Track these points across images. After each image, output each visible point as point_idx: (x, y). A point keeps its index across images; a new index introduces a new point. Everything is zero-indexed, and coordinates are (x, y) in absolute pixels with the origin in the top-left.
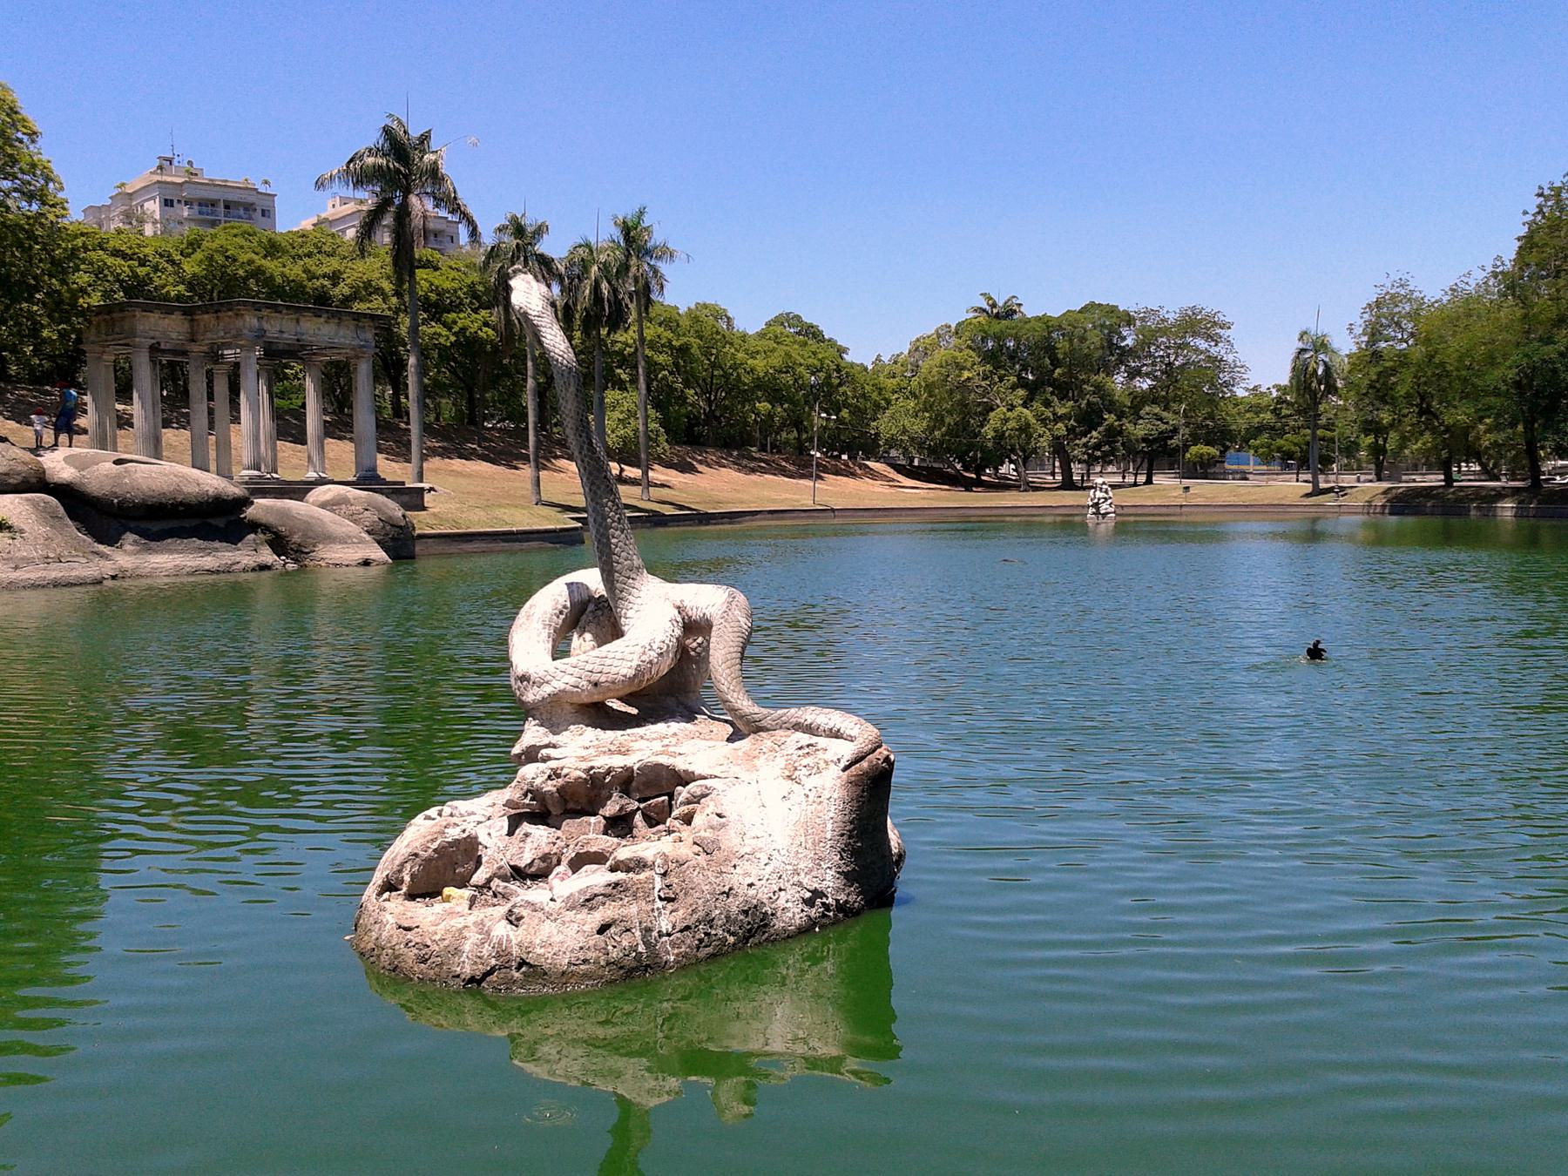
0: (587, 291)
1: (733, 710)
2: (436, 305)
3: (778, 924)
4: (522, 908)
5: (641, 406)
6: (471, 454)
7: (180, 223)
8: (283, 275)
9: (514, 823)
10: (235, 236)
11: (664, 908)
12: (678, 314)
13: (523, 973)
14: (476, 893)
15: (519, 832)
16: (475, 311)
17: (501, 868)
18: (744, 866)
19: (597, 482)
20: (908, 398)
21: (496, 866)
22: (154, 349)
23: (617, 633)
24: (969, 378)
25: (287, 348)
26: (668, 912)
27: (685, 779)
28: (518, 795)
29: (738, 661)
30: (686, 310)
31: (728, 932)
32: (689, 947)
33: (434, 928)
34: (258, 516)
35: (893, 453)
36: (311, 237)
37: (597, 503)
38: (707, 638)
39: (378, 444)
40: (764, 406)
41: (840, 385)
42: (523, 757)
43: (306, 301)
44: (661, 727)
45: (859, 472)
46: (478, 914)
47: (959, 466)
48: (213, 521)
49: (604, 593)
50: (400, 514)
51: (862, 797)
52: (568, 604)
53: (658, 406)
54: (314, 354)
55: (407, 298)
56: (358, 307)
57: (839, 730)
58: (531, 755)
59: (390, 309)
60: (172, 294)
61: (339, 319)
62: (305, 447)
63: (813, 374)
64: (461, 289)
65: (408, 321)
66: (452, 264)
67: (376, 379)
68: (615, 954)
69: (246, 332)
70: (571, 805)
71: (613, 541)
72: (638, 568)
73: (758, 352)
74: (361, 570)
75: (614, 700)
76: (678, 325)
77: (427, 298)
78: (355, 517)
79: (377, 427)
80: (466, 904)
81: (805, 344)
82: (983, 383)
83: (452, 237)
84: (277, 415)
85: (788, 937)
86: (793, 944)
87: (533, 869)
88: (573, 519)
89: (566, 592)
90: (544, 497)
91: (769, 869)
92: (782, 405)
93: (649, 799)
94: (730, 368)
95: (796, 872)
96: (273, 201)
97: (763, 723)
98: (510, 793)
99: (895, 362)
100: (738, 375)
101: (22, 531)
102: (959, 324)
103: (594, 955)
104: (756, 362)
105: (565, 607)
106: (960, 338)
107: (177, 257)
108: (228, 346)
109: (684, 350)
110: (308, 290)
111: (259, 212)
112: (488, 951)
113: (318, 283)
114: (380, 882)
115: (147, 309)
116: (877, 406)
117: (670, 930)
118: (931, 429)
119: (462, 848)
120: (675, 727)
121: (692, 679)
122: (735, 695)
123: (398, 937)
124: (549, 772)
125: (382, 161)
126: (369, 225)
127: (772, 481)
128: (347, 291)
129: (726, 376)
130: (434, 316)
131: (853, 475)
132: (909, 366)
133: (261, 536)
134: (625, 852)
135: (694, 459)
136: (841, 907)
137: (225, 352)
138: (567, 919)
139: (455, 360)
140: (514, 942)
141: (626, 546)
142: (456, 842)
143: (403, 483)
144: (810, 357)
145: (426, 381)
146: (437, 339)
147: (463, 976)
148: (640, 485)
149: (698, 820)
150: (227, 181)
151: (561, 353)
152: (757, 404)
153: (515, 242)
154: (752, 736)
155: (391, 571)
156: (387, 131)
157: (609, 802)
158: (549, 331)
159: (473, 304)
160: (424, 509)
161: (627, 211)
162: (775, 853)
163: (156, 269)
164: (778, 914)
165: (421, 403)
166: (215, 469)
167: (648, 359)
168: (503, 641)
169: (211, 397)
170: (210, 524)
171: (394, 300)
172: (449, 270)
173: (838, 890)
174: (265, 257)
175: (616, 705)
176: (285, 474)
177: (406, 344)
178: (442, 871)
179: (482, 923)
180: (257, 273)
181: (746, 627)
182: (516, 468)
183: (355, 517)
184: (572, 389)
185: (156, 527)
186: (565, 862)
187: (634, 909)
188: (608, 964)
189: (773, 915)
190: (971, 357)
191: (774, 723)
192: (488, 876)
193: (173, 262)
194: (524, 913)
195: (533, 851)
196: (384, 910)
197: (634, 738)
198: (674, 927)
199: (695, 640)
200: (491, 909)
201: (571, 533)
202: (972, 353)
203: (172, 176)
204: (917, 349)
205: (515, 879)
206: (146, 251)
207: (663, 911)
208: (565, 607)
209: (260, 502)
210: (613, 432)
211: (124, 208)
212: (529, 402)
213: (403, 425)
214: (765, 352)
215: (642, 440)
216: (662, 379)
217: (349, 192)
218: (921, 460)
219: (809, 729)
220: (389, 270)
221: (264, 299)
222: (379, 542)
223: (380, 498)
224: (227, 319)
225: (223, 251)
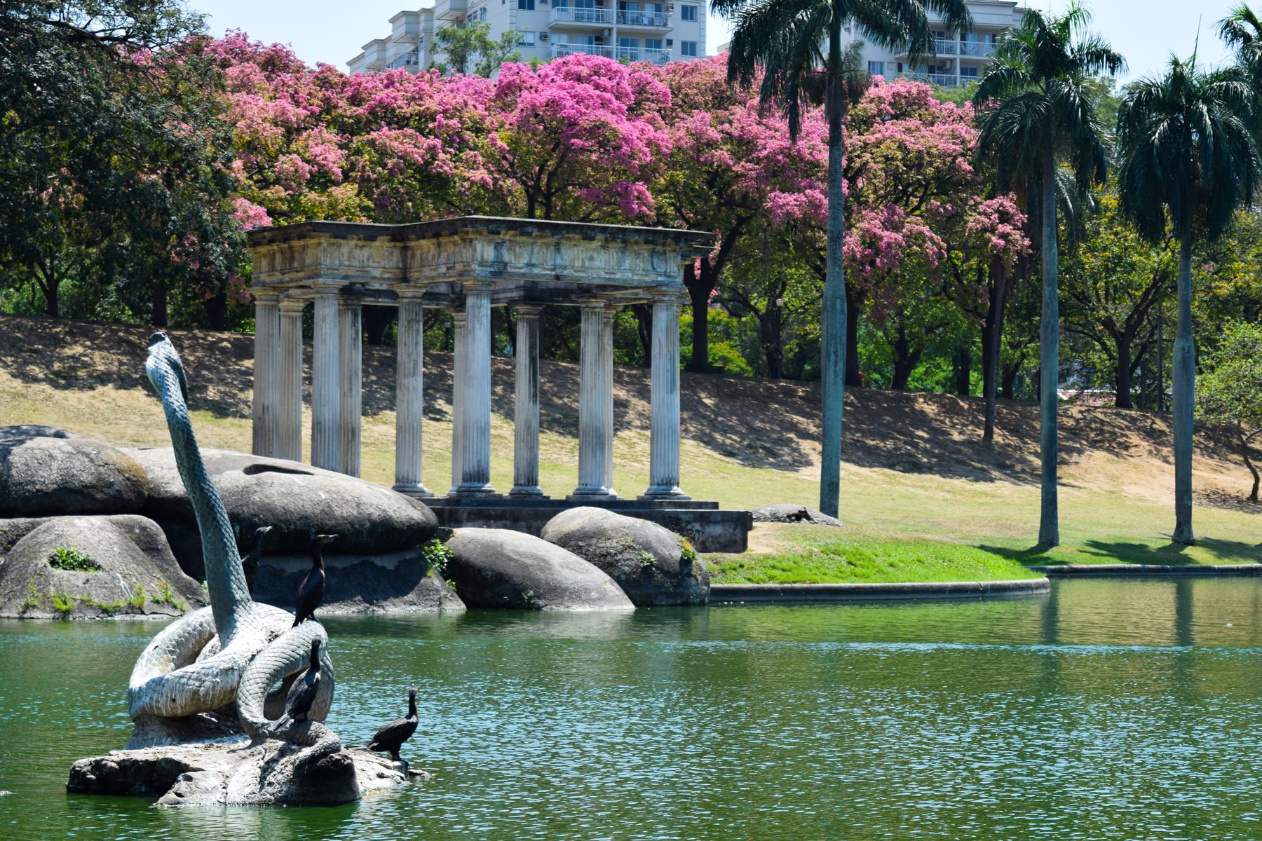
61: (624, 241)
69: (474, 266)
143: (715, 505)
170: (373, 565)
224: (450, 248)
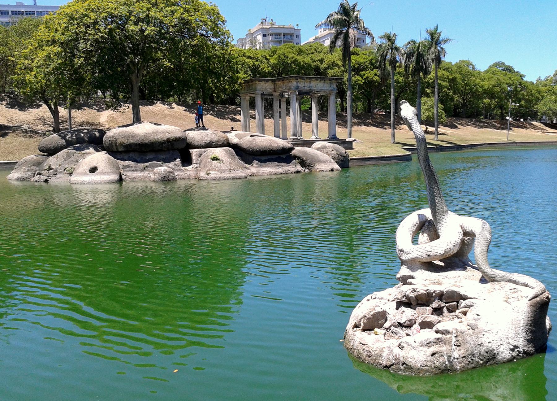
2: (357, 69)
3: (500, 358)
5: (436, 104)
7: (269, 43)
8: (304, 61)
10: (288, 48)
11: (456, 349)
12: (452, 65)
13: (404, 367)
16: (372, 70)
17: (394, 323)
18: (487, 335)
20: (552, 95)
21: (392, 322)
22: (262, 95)
26: (457, 350)
27: (465, 298)
29: (486, 253)
30: (455, 63)
31: (480, 359)
40: (487, 101)
41: (521, 90)
45: (528, 126)
48: (282, 156)
49: (432, 218)
50: (344, 152)
52: (418, 223)
53: (442, 102)
55: (347, 67)
60: (267, 71)
62: (311, 124)
63: (509, 87)
65: (347, 75)
68: (437, 364)
69: (292, 87)
70: (420, 302)
71: (436, 201)
73: (485, 79)
74: (331, 173)
76: (452, 70)
77: (354, 66)
81: (506, 74)
84: (302, 112)
87: (406, 324)
93: (449, 303)
97: (496, 279)
99: (547, 80)
101: (223, 161)
104: (484, 83)
105: (417, 223)
107: (268, 57)
109: (454, 80)
110: (312, 66)
111: (295, 36)
113: (315, 64)
115: (260, 81)
121: (465, 251)
122: (484, 266)
123: (360, 346)
124: (412, 290)
125: (340, 17)
127: (489, 131)
128: (326, 66)
129: (471, 89)
130: (357, 72)
131: (526, 128)
135: (457, 123)
136: (525, 352)
137: (285, 94)
139: (364, 89)
142: (379, 313)
143: (345, 140)
144: (508, 80)
152: (484, 100)
154: (491, 283)
155: (342, 171)
156: (342, 6)
158: (415, 125)
160: (352, 149)
163: (261, 62)
164: (500, 354)
167: (439, 85)
170: (281, 157)
171: (343, 68)
173: (524, 346)
175: (437, 262)
180: (295, 61)
181: (489, 238)
182: (385, 129)
185: (263, 158)
186: (417, 323)
187: (444, 348)
193: (266, 59)
194: (405, 345)
198: (459, 356)
201: (407, 157)
203: (265, 25)
206: (259, 56)
208: (417, 223)
210: (424, 114)
211: (250, 38)
213: (344, 114)
214: (488, 78)
216: (444, 91)
219: (515, 282)
220: (341, 57)
222: (336, 162)
224: (286, 83)
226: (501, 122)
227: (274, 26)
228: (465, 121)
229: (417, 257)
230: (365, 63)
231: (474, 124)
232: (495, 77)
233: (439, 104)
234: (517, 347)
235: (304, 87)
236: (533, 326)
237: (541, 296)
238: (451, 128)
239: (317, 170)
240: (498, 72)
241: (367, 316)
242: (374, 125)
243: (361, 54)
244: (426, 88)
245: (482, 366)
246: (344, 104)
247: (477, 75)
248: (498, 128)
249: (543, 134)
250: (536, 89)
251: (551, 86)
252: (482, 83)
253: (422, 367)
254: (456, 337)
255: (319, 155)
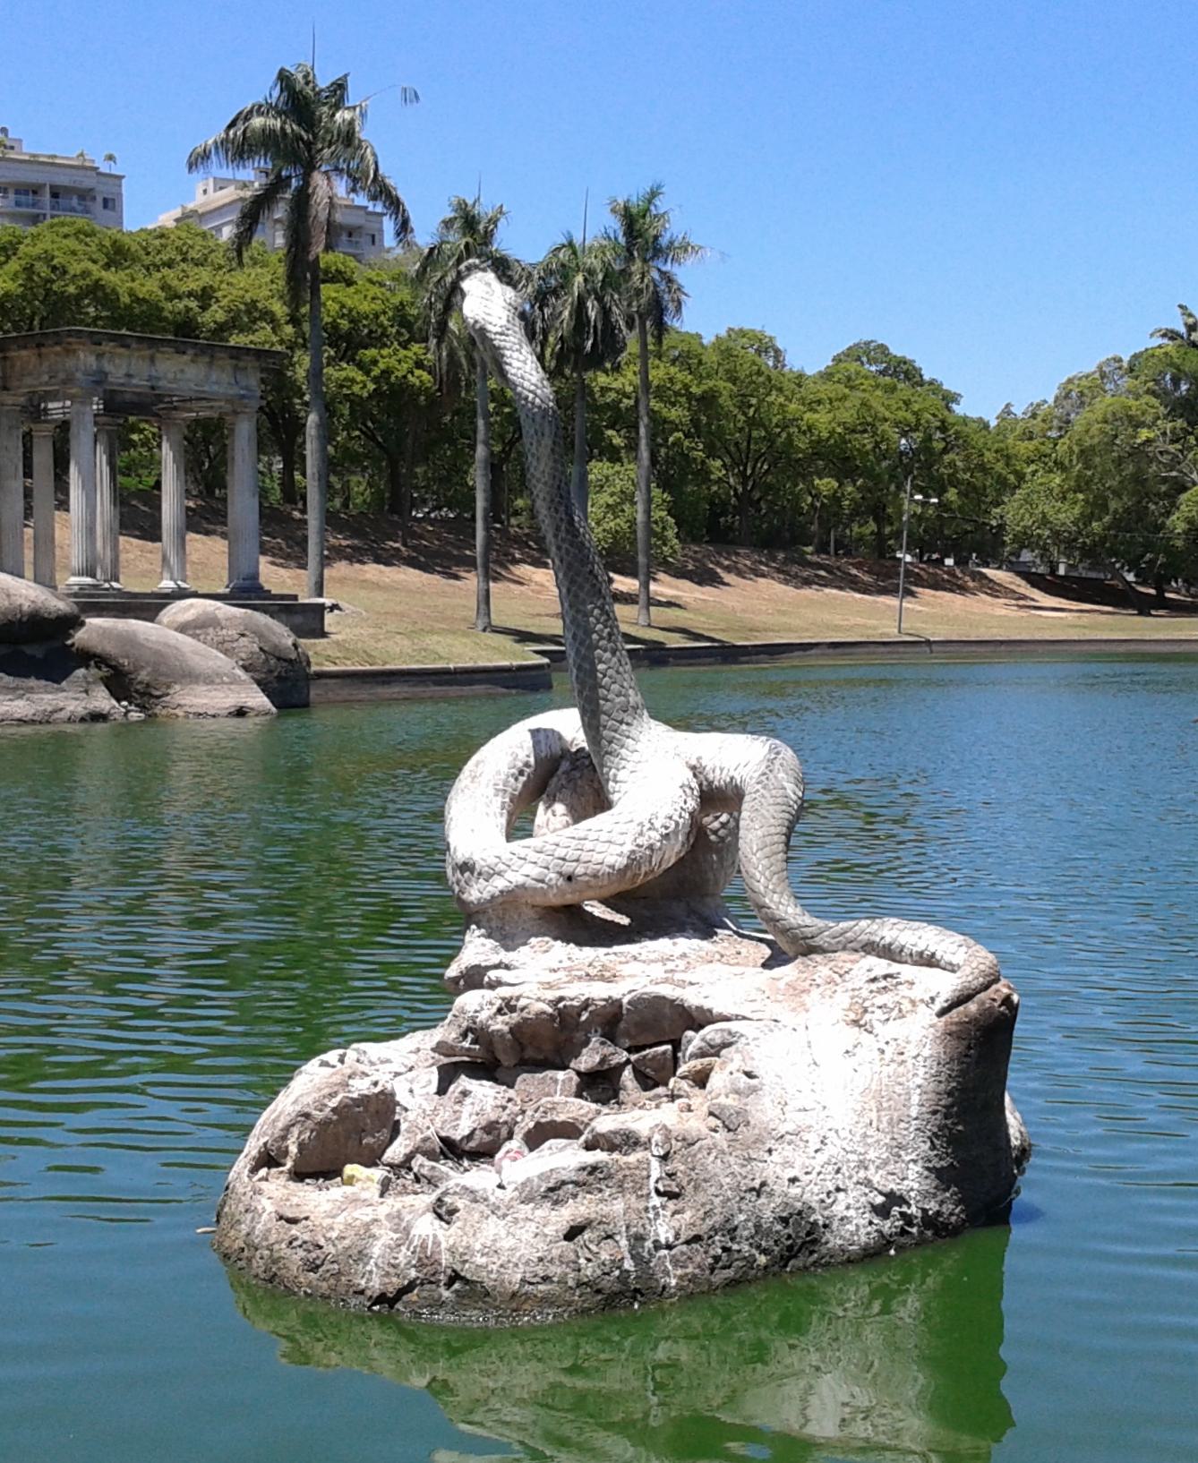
0: (566, 313)
1: (773, 920)
2: (348, 337)
3: (834, 1241)
4: (457, 1197)
5: (643, 485)
6: (393, 556)
8: (131, 293)
9: (447, 1076)
10: (66, 236)
11: (664, 1207)
13: (456, 1291)
14: (391, 1175)
15: (455, 1089)
17: (426, 1140)
18: (783, 1152)
19: (580, 580)
20: (1051, 471)
21: (420, 1137)
23: (601, 803)
24: (1148, 441)
25: (135, 399)
26: (668, 1213)
27: (697, 1019)
28: (454, 1035)
29: (781, 847)
30: (713, 339)
31: (758, 1247)
32: (699, 1267)
33: (329, 1221)
34: (90, 644)
35: (1026, 556)
36: (172, 237)
37: (578, 611)
38: (736, 814)
39: (262, 544)
40: (826, 484)
41: (945, 451)
42: (462, 982)
43: (165, 330)
44: (663, 945)
45: (971, 584)
46: (393, 1203)
47: (1130, 577)
49: (585, 745)
50: (290, 642)
51: (966, 1056)
52: (532, 760)
53: (665, 484)
54: (175, 408)
55: (306, 327)
56: (236, 340)
57: (933, 955)
58: (474, 978)
59: (282, 342)
61: (212, 356)
62: (158, 545)
63: (904, 434)
64: (384, 313)
65: (307, 360)
66: (372, 275)
67: (261, 449)
68: (589, 1271)
69: (79, 375)
70: (530, 1053)
71: (601, 667)
72: (635, 708)
73: (819, 402)
75: (595, 903)
76: (700, 363)
77: (335, 326)
78: (227, 645)
79: (261, 518)
80: (375, 1189)
82: (1171, 448)
83: (373, 236)
84: (121, 498)
85: (849, 1261)
86: (853, 1272)
87: (472, 1144)
88: (537, 652)
89: (529, 743)
90: (496, 620)
91: (821, 1158)
92: (854, 482)
93: (643, 1048)
94: (777, 426)
95: (863, 1165)
96: (120, 186)
97: (818, 941)
98: (444, 1032)
99: (1034, 416)
100: (789, 435)
102: (1136, 356)
103: (559, 1271)
104: (816, 416)
105: (527, 765)
106: (1137, 378)
108: (54, 396)
110: (166, 314)
111: (100, 200)
112: (406, 1257)
113: (180, 305)
114: (254, 1153)
116: (1002, 483)
117: (671, 1239)
118: (1087, 519)
119: (372, 1109)
120: (683, 944)
121: (710, 875)
122: (776, 897)
123: (280, 1232)
124: (498, 1003)
126: (252, 214)
127: (835, 598)
128: (221, 316)
129: (770, 439)
131: (962, 589)
132: (1055, 422)
133: (94, 671)
134: (607, 1121)
135: (718, 564)
136: (929, 1221)
137: (51, 406)
138: (521, 1216)
140: (444, 1245)
141: (619, 680)
142: (364, 1100)
143: (295, 597)
144: (899, 408)
145: (330, 449)
146: (349, 388)
147: (369, 1293)
148: (637, 603)
149: (717, 1081)
150: (55, 157)
151: (532, 388)
152: (817, 481)
153: (463, 241)
154: (800, 960)
155: (279, 716)
156: (284, 78)
157: (584, 1051)
158: (516, 355)
159: (402, 334)
160: (324, 635)
161: (631, 191)
162: (832, 1134)
164: (835, 1225)
165: (323, 481)
166: (32, 577)
167: (653, 414)
168: (439, 816)
169: (28, 473)
171: (289, 329)
172: (368, 285)
173: (925, 1195)
174: (107, 266)
175: (598, 910)
176: (130, 583)
177: (304, 394)
178: (342, 1140)
179: (399, 1216)
180: (97, 291)
182: (457, 577)
183: (226, 645)
184: (547, 441)
187: (618, 1206)
188: (580, 1284)
189: (825, 1226)
190: (1152, 407)
191: (833, 941)
192: (408, 1151)
194: (460, 1204)
195: (474, 1117)
196: (259, 1192)
197: (623, 959)
198: (677, 1236)
199: (717, 818)
200: (413, 1196)
201: (533, 673)
202: (1154, 401)
204: (1067, 396)
205: (446, 1158)
207: (661, 1212)
209: (94, 622)
210: (598, 523)
212: (478, 478)
213: (297, 514)
215: (640, 534)
216: (674, 444)
217: (227, 173)
218: (1070, 567)
219: (888, 952)
221: (103, 327)
222: (259, 683)
223: (262, 619)
225: (48, 258)
226: (876, 569)
227: (12, 155)
228: (747, 557)
229: (523, 887)
230: (377, 316)
231: (779, 571)
232: (855, 398)
233: (656, 492)
234: (900, 1200)
235: (129, 376)
236: (958, 1115)
237: (982, 995)
238: (700, 583)
239: (177, 711)
240: (866, 378)
241: (315, 1113)
242: (412, 563)
243: (360, 282)
244: (607, 427)
245: (765, 1276)
246: (297, 476)
247: (793, 386)
248: (865, 589)
249: (1023, 613)
250: (996, 446)
251: (1049, 438)
252: (807, 416)
253: (527, 1288)
254: (664, 1158)
255: (186, 649)
